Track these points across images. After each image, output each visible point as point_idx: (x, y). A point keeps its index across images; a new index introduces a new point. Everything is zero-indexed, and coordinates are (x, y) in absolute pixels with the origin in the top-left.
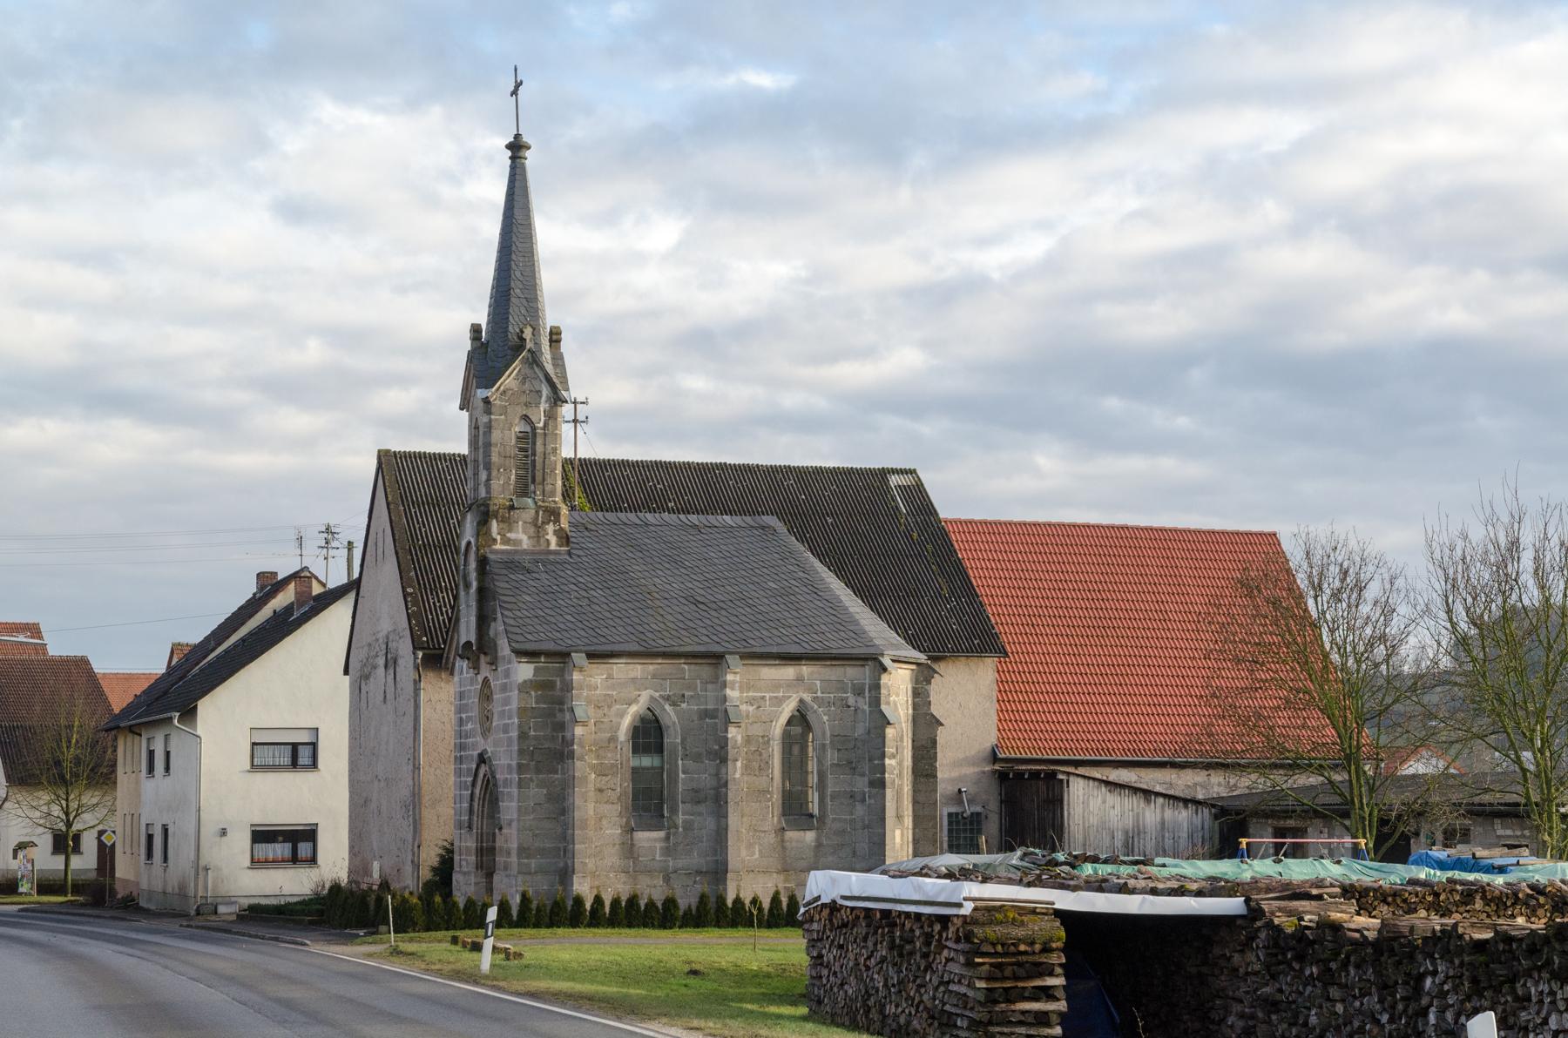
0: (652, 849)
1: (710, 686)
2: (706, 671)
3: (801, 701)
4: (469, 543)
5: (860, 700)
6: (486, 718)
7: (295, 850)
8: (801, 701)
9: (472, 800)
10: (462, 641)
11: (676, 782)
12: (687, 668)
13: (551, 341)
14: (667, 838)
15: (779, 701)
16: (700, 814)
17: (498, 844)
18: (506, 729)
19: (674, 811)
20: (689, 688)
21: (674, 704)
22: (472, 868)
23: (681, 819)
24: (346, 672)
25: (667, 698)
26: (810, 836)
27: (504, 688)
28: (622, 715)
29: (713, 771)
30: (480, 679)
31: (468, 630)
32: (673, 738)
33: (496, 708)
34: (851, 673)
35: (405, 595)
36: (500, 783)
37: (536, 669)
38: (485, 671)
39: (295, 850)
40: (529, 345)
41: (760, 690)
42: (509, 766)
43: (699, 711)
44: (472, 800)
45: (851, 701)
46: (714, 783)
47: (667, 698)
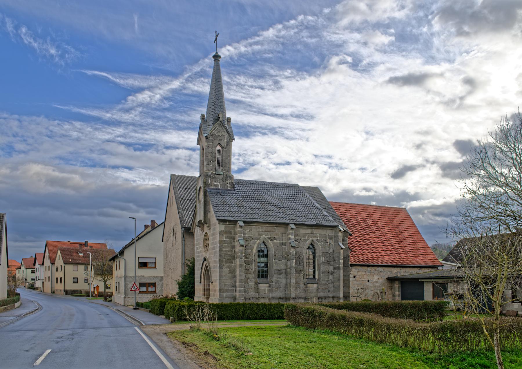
0: (265, 290)
1: (283, 235)
2: (282, 230)
3: (313, 241)
4: (200, 188)
5: (331, 241)
6: (206, 246)
7: (147, 289)
8: (313, 241)
9: (201, 273)
10: (198, 220)
11: (273, 267)
12: (276, 229)
13: (228, 122)
14: (270, 286)
15: (305, 240)
16: (280, 278)
17: (211, 288)
18: (214, 248)
19: (272, 277)
20: (277, 235)
21: (272, 240)
22: (201, 295)
23: (274, 279)
24: (163, 241)
25: (270, 238)
26: (315, 286)
27: (213, 234)
28: (254, 244)
29: (285, 264)
30: (204, 233)
31: (200, 216)
32: (271, 253)
33: (210, 242)
34: (329, 232)
35: (179, 212)
36: (212, 267)
37: (225, 227)
38: (206, 230)
39: (147, 289)
40: (221, 119)
41: (299, 236)
42: (215, 261)
43: (280, 243)
44: (201, 273)
45: (328, 241)
46: (285, 268)
47: (270, 238)
